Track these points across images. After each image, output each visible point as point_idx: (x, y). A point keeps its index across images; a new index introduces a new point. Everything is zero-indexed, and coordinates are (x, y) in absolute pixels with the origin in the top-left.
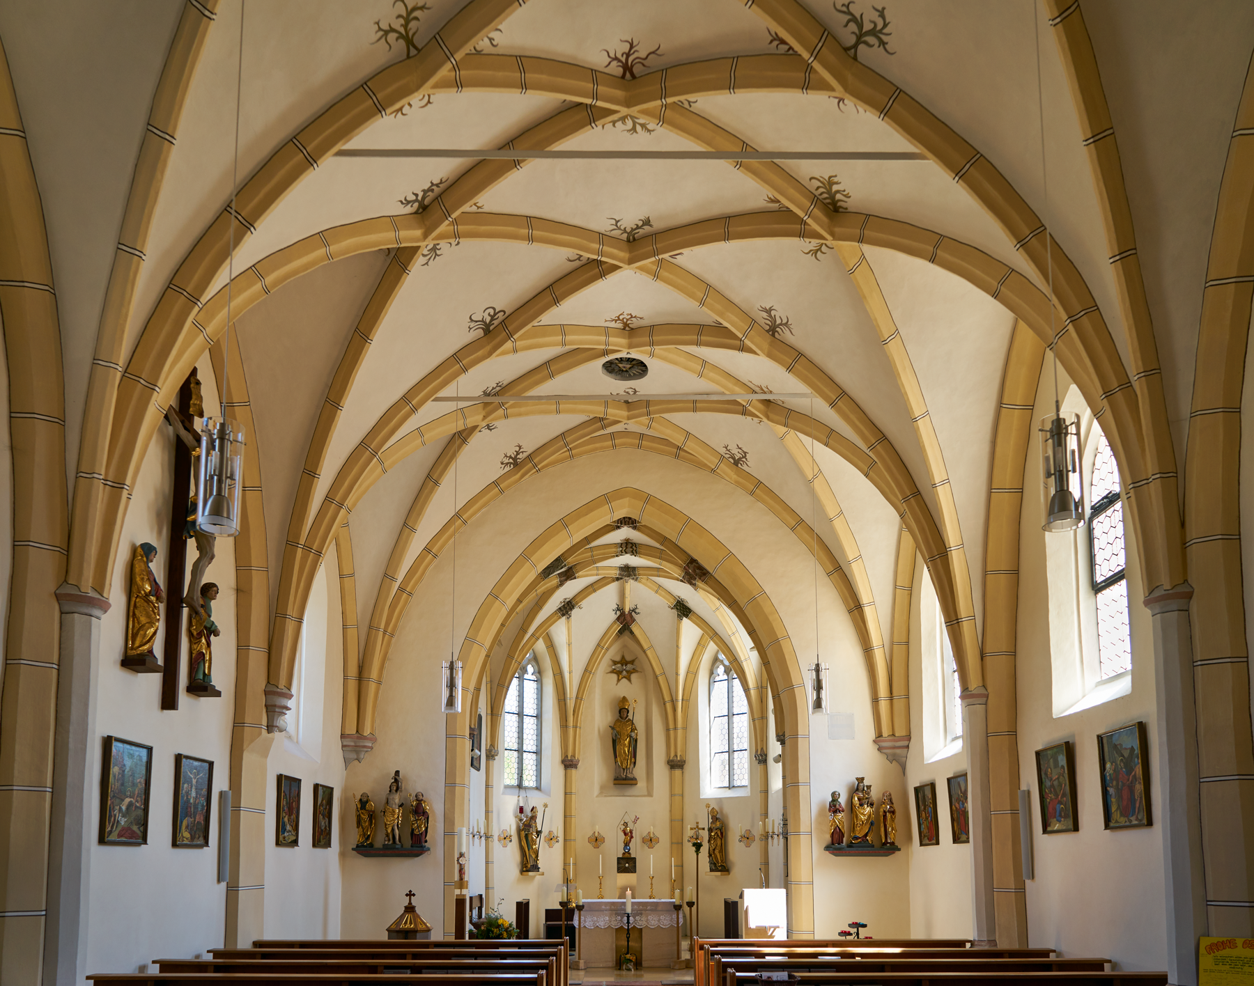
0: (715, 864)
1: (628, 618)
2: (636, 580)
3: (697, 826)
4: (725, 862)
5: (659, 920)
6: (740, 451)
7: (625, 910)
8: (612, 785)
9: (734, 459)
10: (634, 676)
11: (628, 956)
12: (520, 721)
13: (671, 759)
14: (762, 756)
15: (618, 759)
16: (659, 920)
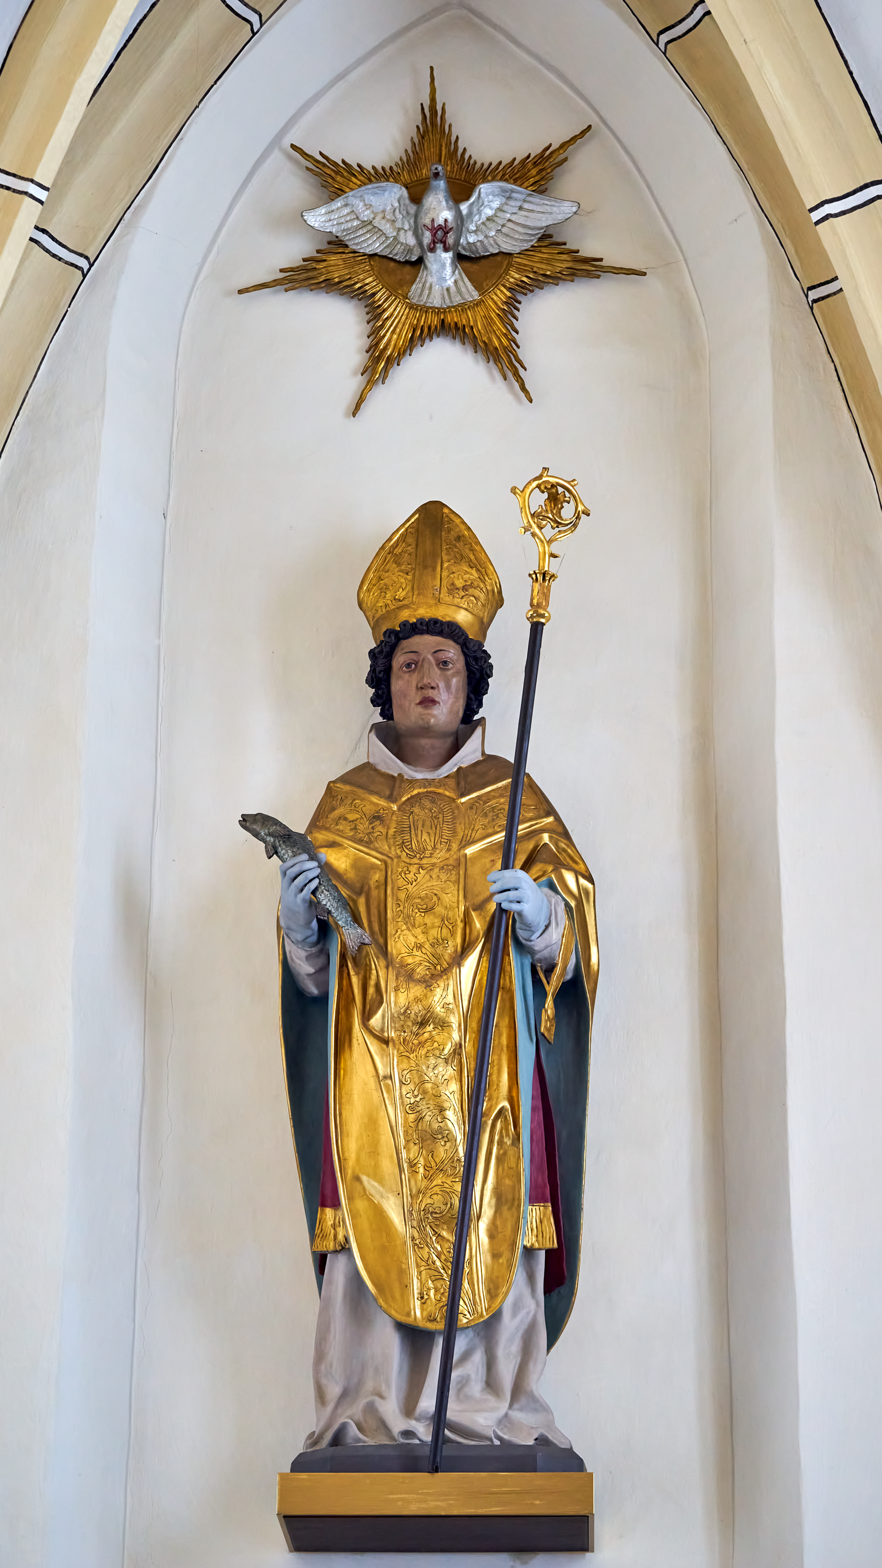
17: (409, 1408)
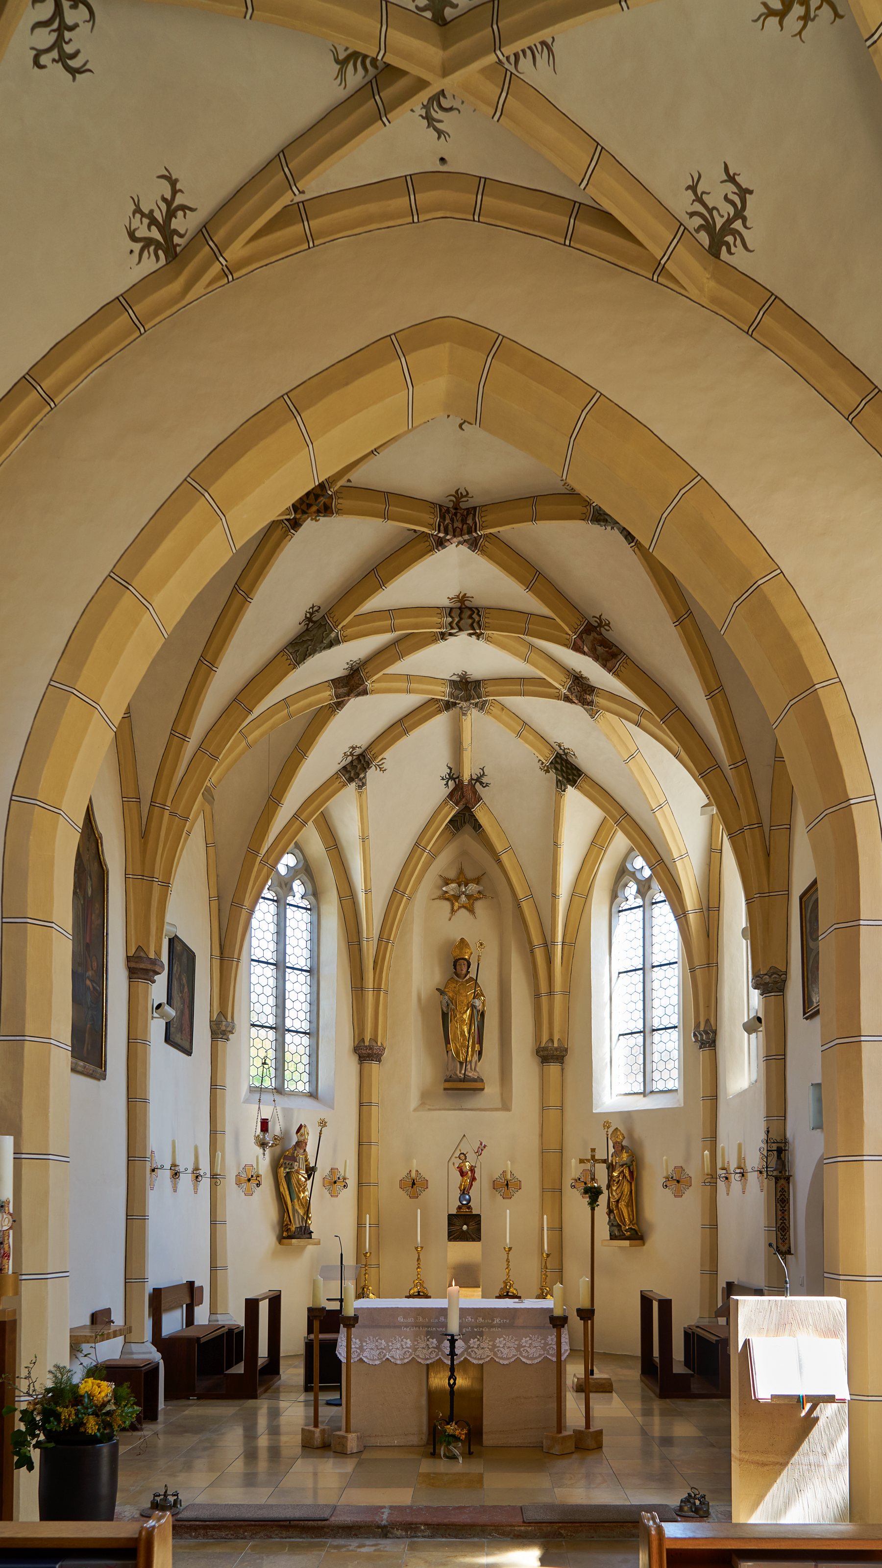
0: (619, 1226)
1: (469, 794)
2: (482, 709)
3: (593, 1157)
4: (637, 1223)
5: (519, 1348)
6: (731, 187)
7: (445, 1325)
8: (442, 1091)
9: (708, 227)
10: (479, 906)
11: (451, 1428)
12: (280, 978)
13: (543, 1045)
14: (707, 1033)
15: (452, 1046)
16: (520, 1346)
17: (460, 1073)
